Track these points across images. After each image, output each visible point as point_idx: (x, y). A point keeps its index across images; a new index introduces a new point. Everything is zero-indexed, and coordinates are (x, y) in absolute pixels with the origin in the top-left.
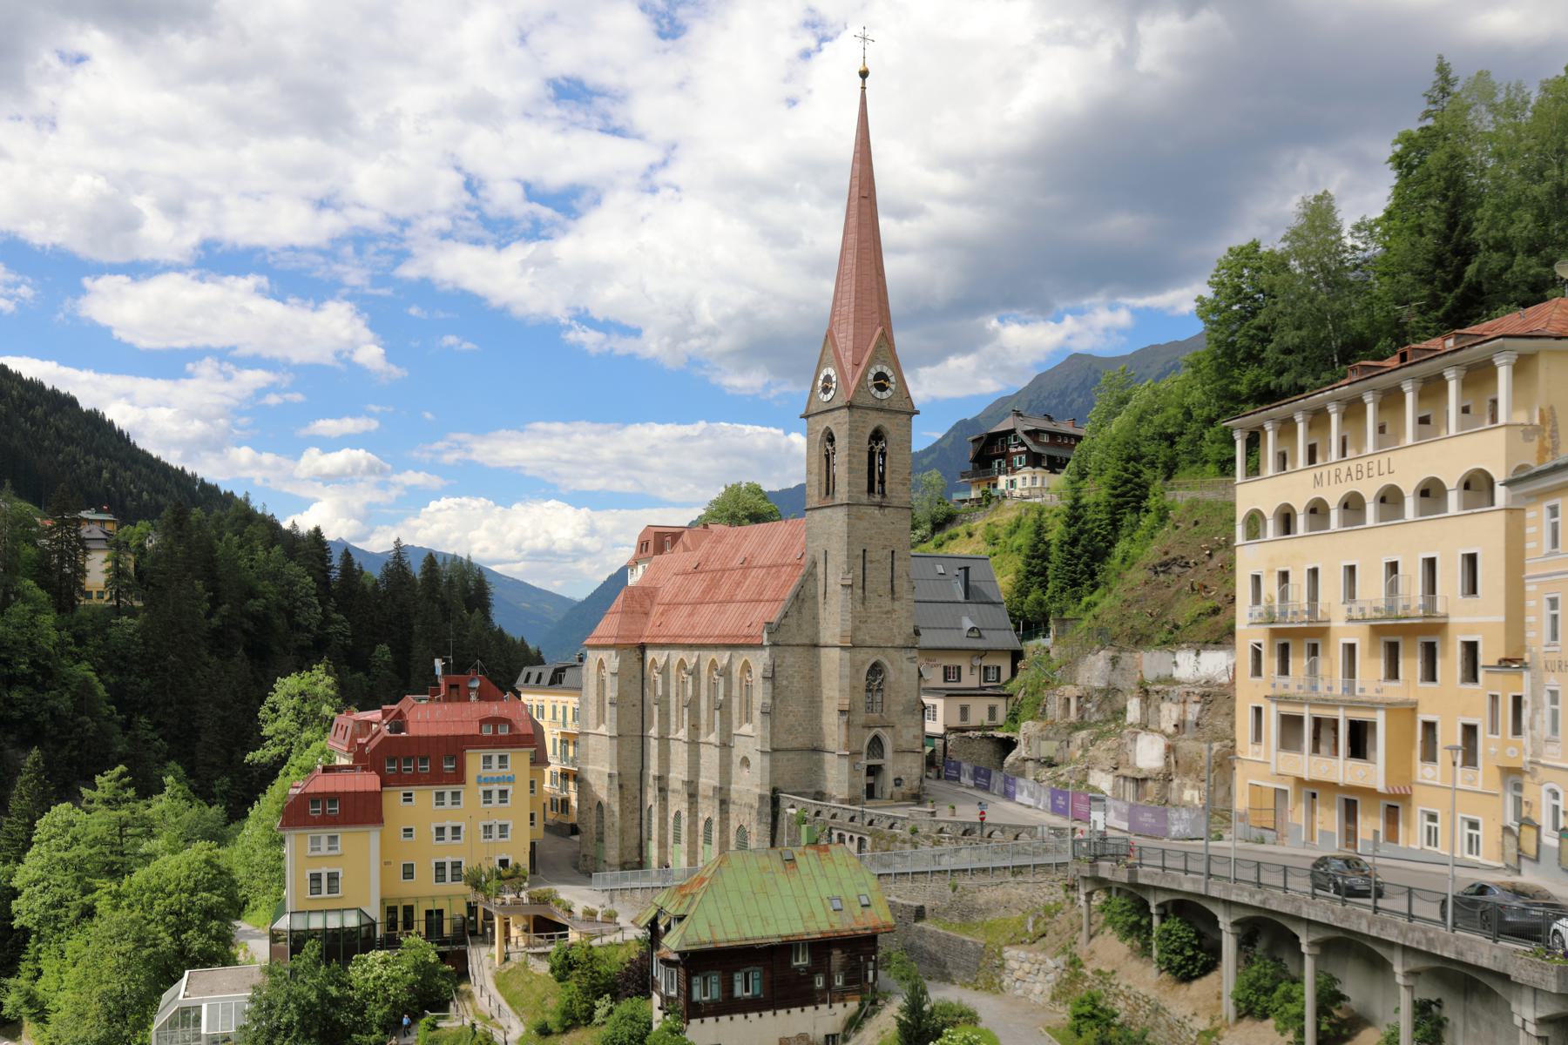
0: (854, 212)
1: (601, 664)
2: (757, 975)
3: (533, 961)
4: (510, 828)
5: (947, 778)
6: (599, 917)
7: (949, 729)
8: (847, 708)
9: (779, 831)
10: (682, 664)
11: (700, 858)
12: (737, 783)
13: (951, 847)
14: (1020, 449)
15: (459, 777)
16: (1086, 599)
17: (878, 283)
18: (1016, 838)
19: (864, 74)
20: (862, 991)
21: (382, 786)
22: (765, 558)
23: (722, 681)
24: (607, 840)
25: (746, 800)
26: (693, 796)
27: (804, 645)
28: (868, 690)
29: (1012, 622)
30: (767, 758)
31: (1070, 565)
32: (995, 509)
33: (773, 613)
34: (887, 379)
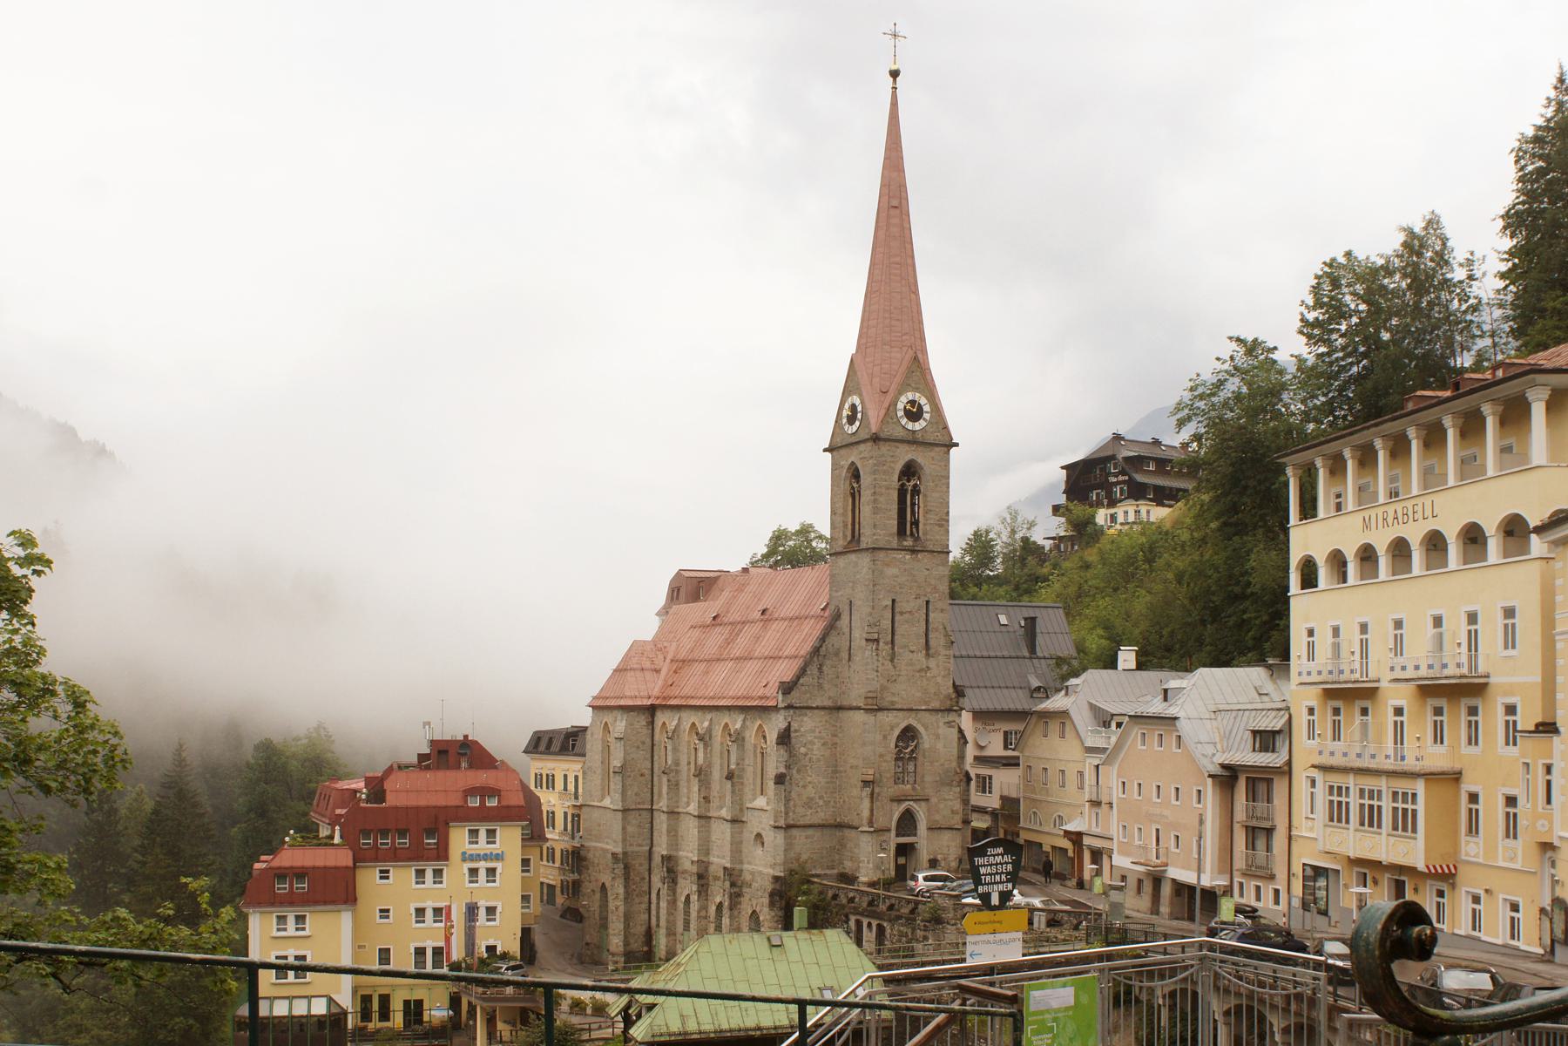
4: (499, 910)
8: (870, 778)
14: (1121, 478)
15: (442, 853)
19: (895, 74)
21: (355, 860)
22: (790, 609)
24: (611, 925)
27: (823, 708)
33: (785, 671)
34: (920, 407)
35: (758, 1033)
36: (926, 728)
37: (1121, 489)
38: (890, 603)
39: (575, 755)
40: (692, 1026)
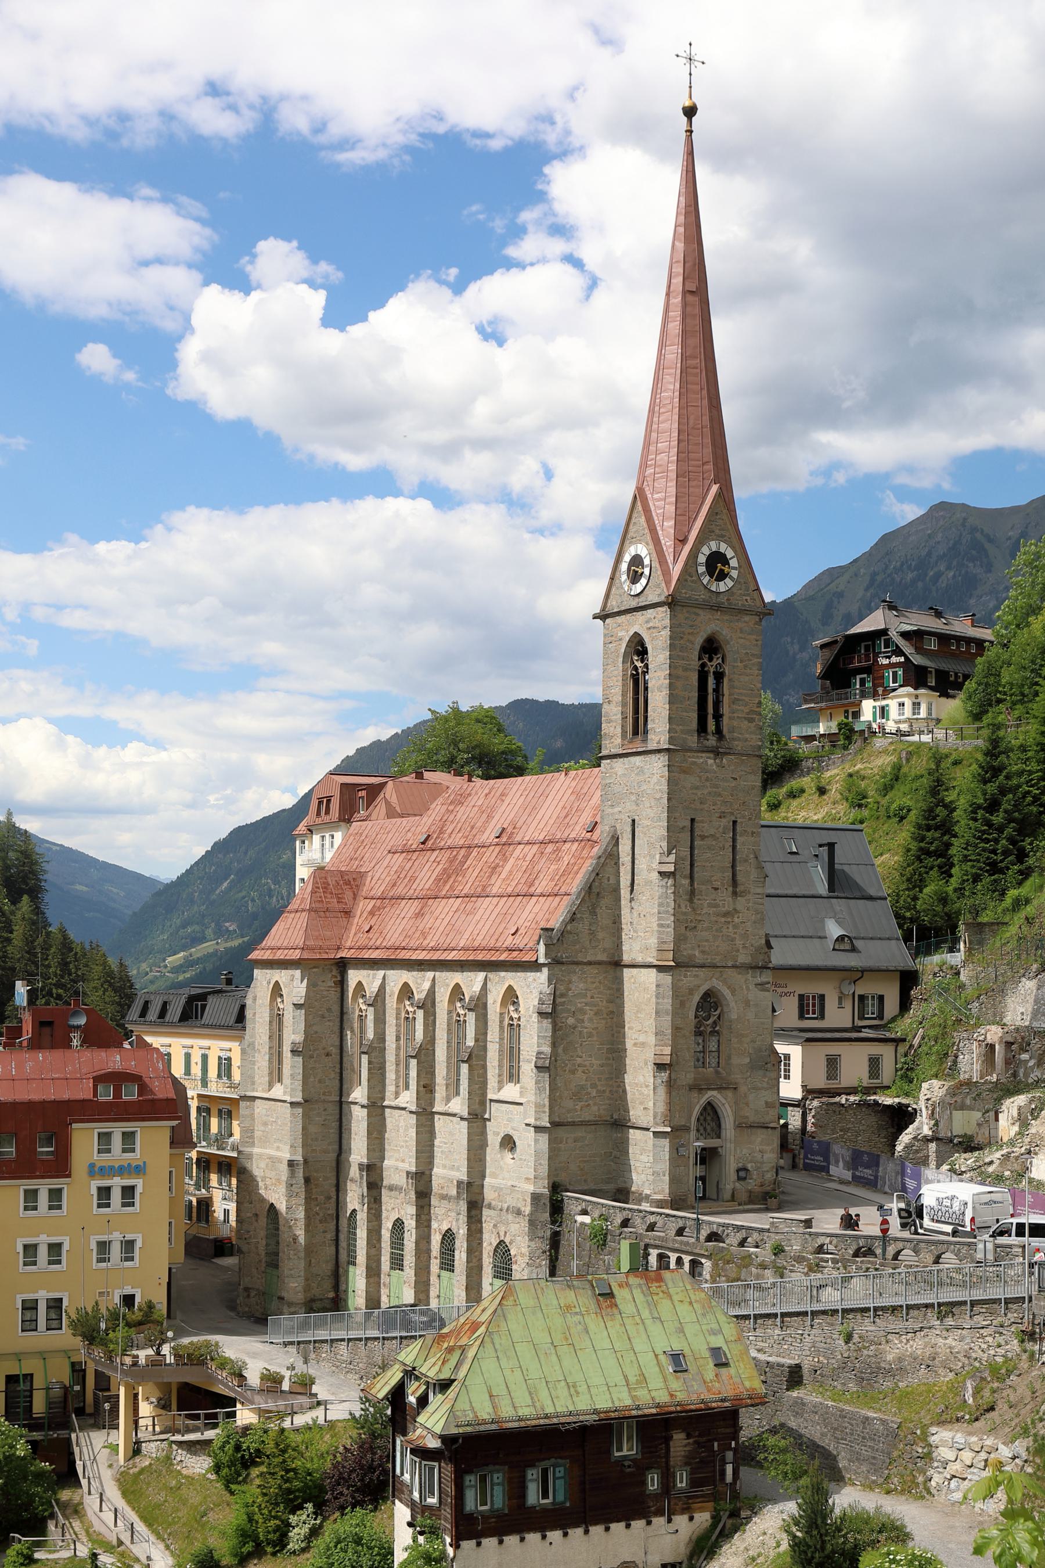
0: (676, 314)
1: (277, 990)
2: (560, 1472)
3: (180, 1454)
5: (808, 1168)
6: (286, 1386)
7: (809, 1092)
8: (667, 1060)
9: (562, 1251)
10: (406, 991)
11: (433, 1292)
12: (494, 1176)
13: (835, 1274)
14: (895, 659)
15: (60, 1166)
16: (1013, 893)
17: (711, 419)
18: (937, 1261)
19: (690, 112)
20: (716, 1497)
22: (534, 831)
23: (471, 1018)
25: (510, 1201)
26: (423, 1196)
27: (599, 963)
28: (698, 1033)
29: (900, 926)
30: (544, 1139)
31: (987, 841)
32: (861, 750)
34: (725, 561)
35: (595, 1417)
36: (733, 992)
37: (895, 674)
38: (688, 824)
39: (204, 1026)
40: (506, 1411)
